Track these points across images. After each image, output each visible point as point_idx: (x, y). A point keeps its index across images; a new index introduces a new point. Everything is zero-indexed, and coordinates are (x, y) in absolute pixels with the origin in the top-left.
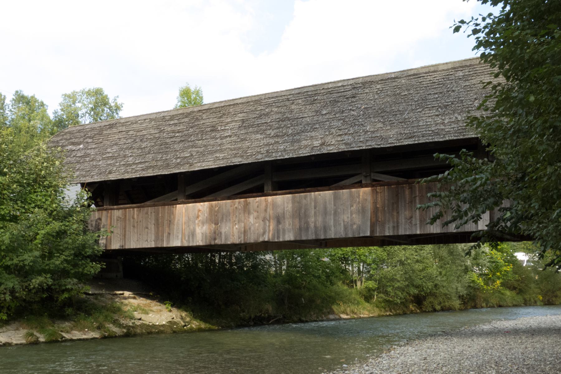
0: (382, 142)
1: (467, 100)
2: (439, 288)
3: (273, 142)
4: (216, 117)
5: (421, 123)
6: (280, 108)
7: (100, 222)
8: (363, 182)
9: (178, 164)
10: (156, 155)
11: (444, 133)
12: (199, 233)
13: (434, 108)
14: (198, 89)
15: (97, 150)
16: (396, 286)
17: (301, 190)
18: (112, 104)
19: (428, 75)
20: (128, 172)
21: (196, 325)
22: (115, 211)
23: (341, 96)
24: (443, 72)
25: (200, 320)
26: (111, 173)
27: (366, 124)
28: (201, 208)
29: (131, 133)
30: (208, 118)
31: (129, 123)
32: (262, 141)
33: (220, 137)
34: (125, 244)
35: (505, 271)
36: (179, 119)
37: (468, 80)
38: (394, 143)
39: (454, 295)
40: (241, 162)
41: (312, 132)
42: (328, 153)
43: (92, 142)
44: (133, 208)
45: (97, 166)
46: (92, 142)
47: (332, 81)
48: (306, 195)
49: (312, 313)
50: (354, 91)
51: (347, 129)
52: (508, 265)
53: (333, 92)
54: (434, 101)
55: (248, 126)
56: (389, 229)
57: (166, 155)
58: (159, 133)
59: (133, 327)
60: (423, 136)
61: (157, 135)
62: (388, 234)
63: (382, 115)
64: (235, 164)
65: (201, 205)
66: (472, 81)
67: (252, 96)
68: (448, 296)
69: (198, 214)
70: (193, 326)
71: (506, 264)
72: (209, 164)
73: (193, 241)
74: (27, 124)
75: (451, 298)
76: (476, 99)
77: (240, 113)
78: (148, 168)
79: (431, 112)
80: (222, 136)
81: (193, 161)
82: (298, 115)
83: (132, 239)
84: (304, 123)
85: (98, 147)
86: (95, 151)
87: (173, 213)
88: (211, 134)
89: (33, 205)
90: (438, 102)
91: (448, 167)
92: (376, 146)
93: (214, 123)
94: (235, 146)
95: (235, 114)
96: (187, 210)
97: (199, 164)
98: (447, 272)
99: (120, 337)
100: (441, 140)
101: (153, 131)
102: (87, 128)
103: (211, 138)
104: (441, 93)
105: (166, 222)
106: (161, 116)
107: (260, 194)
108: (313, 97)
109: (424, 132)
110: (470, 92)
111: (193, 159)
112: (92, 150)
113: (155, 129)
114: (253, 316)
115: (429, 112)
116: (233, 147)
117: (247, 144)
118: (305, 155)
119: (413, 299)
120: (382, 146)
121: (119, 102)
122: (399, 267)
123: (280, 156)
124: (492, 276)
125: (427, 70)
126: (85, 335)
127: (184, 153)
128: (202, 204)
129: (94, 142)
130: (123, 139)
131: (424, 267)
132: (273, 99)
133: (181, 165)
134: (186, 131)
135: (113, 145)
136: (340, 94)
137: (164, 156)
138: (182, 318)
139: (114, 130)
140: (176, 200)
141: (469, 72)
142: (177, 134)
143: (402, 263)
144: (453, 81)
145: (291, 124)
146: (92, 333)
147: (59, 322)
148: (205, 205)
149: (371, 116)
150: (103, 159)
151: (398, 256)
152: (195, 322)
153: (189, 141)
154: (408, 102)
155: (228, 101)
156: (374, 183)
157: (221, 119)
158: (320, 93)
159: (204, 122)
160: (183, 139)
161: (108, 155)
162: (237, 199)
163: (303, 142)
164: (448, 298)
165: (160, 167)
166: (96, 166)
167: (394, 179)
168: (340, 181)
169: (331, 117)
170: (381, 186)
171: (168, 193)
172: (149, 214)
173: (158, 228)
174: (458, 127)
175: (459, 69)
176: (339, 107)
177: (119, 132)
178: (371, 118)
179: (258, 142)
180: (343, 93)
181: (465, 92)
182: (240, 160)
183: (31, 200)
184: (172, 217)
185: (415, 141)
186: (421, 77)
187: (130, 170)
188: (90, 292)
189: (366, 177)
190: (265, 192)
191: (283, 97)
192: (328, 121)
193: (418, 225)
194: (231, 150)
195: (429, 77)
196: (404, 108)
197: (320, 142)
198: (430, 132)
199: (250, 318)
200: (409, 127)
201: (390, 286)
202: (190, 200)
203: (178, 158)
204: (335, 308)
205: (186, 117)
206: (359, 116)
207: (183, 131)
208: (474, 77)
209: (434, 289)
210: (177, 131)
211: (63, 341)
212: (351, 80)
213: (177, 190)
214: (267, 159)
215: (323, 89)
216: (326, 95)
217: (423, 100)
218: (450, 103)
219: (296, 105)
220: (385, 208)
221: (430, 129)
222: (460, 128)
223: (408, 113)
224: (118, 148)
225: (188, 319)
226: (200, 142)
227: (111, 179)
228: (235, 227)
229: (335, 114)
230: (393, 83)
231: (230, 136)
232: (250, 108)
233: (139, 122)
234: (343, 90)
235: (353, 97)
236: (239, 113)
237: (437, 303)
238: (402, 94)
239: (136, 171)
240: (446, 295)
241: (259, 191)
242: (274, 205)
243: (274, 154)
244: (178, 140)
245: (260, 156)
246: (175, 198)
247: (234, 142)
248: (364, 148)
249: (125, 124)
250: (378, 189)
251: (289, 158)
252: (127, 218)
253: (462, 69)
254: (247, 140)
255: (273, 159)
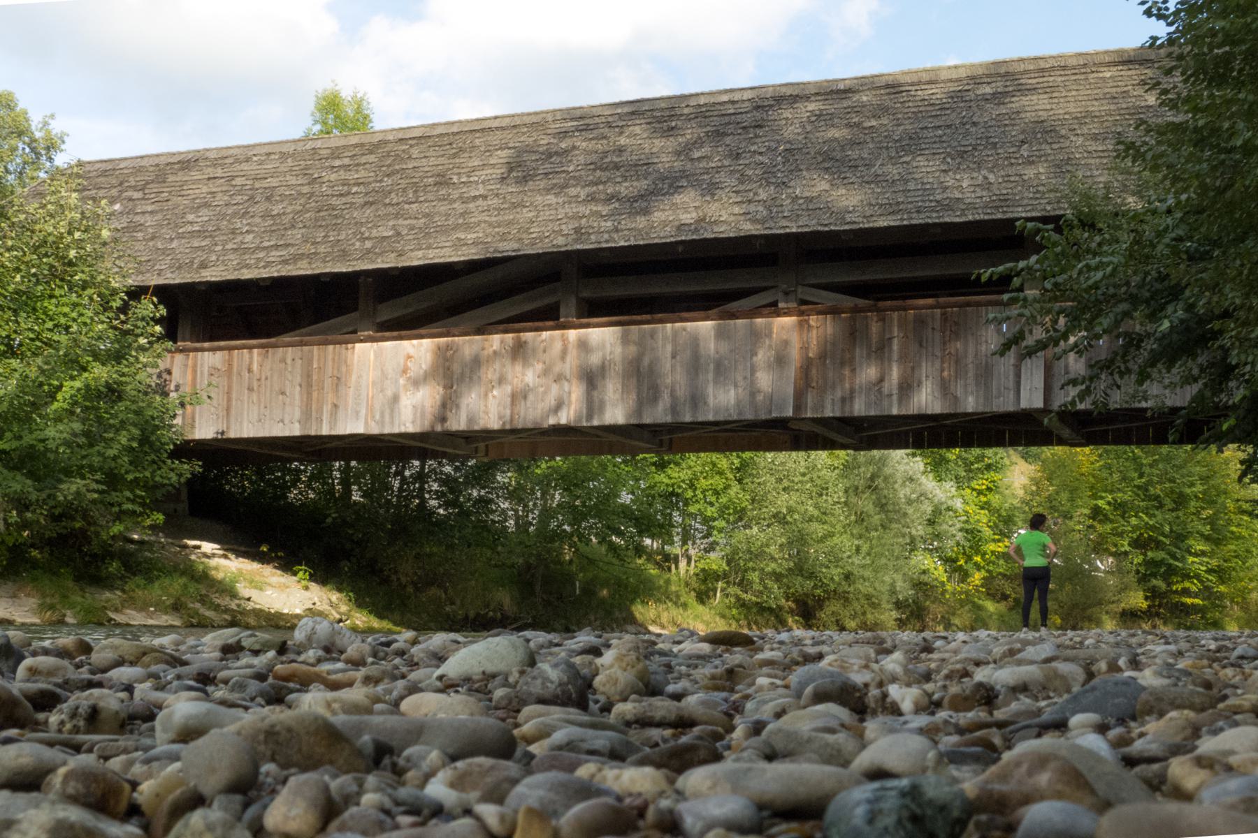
0: (832, 221)
1: (1004, 143)
2: (854, 583)
3: (588, 212)
4: (443, 156)
5: (911, 186)
6: (593, 142)
7: (168, 377)
8: (781, 305)
9: (368, 251)
10: (310, 231)
11: (964, 207)
12: (406, 407)
13: (937, 157)
14: (359, 95)
15: (159, 216)
16: (769, 569)
17: (645, 317)
18: (38, 135)
19: (918, 88)
20: (248, 266)
21: (364, 622)
22: (206, 353)
23: (729, 123)
24: (949, 84)
25: (370, 612)
26: (206, 267)
27: (792, 184)
28: (411, 351)
29: (238, 181)
30: (425, 157)
31: (230, 160)
32: (560, 210)
33: (461, 198)
34: (228, 428)
35: (993, 552)
36: (355, 155)
37: (1004, 104)
38: (859, 223)
39: (885, 597)
40: (519, 250)
41: (672, 194)
42: (716, 239)
43: (143, 199)
44: (250, 348)
45: (168, 252)
46: (143, 199)
47: (706, 90)
48: (654, 329)
49: (592, 618)
50: (757, 114)
51: (750, 190)
52: (999, 541)
53: (711, 114)
54: (935, 142)
55: (524, 177)
56: (833, 404)
57: (336, 233)
58: (309, 184)
59: (241, 613)
60: (918, 212)
61: (305, 189)
62: (831, 415)
63: (826, 165)
64: (505, 254)
65: (414, 346)
66: (1013, 105)
67: (522, 115)
68: (874, 600)
69: (405, 365)
70: (357, 622)
71: (997, 537)
72: (443, 252)
73: (392, 423)
75: (879, 605)
76: (1023, 142)
77: (500, 149)
78: (296, 258)
79: (931, 164)
80: (465, 195)
81: (404, 246)
82: (637, 158)
83: (245, 416)
84: (654, 176)
85: (162, 210)
86: (156, 218)
87: (346, 362)
88: (438, 191)
89: (50, 325)
90: (945, 145)
91: (1038, 248)
92: (820, 228)
93: (440, 167)
94: (500, 218)
95: (488, 151)
96: (378, 355)
97: (420, 254)
98: (871, 548)
100: (958, 220)
101: (293, 181)
102: (121, 166)
103: (440, 200)
104: (949, 127)
105: (328, 382)
106: (308, 147)
107: (550, 323)
108: (665, 121)
109: (920, 204)
110: (1011, 128)
111: (402, 242)
112: (148, 217)
113: (297, 176)
114: (472, 614)
115: (926, 164)
116: (494, 219)
117: (527, 214)
118: (664, 241)
119: (793, 606)
120: (833, 228)
121: (56, 127)
122: (777, 528)
123: (607, 241)
124: (966, 563)
125: (915, 79)
126: (152, 618)
127: (380, 229)
128: (415, 342)
129: (148, 199)
130: (220, 194)
131: (826, 532)
132: (575, 123)
133: (376, 253)
134: (377, 182)
135: (199, 207)
136: (727, 119)
137: (331, 233)
138: (331, 604)
139: (195, 175)
140: (355, 332)
141: (1006, 86)
142: (354, 189)
143: (779, 518)
144: (972, 103)
145: (622, 176)
146: (165, 617)
147: (93, 589)
148: (421, 345)
149: (802, 167)
150: (180, 236)
151: (773, 503)
152: (358, 615)
153: (386, 205)
154: (880, 142)
155: (467, 121)
156: (804, 307)
157: (457, 160)
158: (681, 115)
159: (416, 164)
160: (371, 199)
161: (190, 228)
162: (496, 333)
163: (656, 214)
164: (874, 603)
165: (326, 257)
166: (164, 251)
167: (848, 301)
168: (734, 300)
169: (713, 165)
170: (819, 313)
171: (304, 327)
172: (289, 361)
173: (309, 394)
174: (990, 197)
175: (983, 80)
176: (728, 145)
177: (209, 179)
178: (801, 170)
179: (553, 212)
180: (733, 117)
181: (999, 126)
182: (516, 246)
183: (45, 313)
184: (344, 369)
185: (902, 219)
186: (902, 92)
187: (252, 262)
188: (136, 537)
189: (786, 293)
190: (562, 320)
191: (597, 120)
192: (707, 173)
193: (895, 398)
194: (490, 224)
195: (919, 93)
196: (873, 153)
197: (694, 215)
198: (933, 204)
199: (467, 617)
200: (887, 192)
201: (754, 570)
202: (387, 334)
203: (367, 238)
204: (638, 610)
205: (371, 153)
206: (775, 166)
207: (370, 183)
208: (1017, 99)
209: (844, 583)
210: (352, 182)
212: (749, 91)
213: (356, 309)
214: (579, 247)
215: (687, 106)
216: (696, 120)
217: (911, 138)
218: (970, 148)
219: (628, 137)
220: (825, 361)
221: (931, 198)
222: (994, 198)
223: (882, 165)
224: (212, 213)
225: (344, 608)
226: (412, 206)
227: (209, 279)
228: (490, 395)
229: (720, 160)
230: (844, 101)
231: (485, 197)
232: (522, 139)
233: (255, 159)
234: (732, 111)
235: (756, 127)
236: (497, 150)
237: (848, 614)
238: (867, 124)
239: (268, 265)
240: (868, 597)
241: (548, 316)
242: (583, 345)
243: (592, 237)
244: (359, 200)
245: (560, 241)
246: (351, 329)
247: (494, 208)
248: (794, 230)
249: (220, 162)
250: (813, 320)
251: (630, 246)
252: (235, 370)
253: (989, 80)
254: (525, 207)
255: (591, 246)
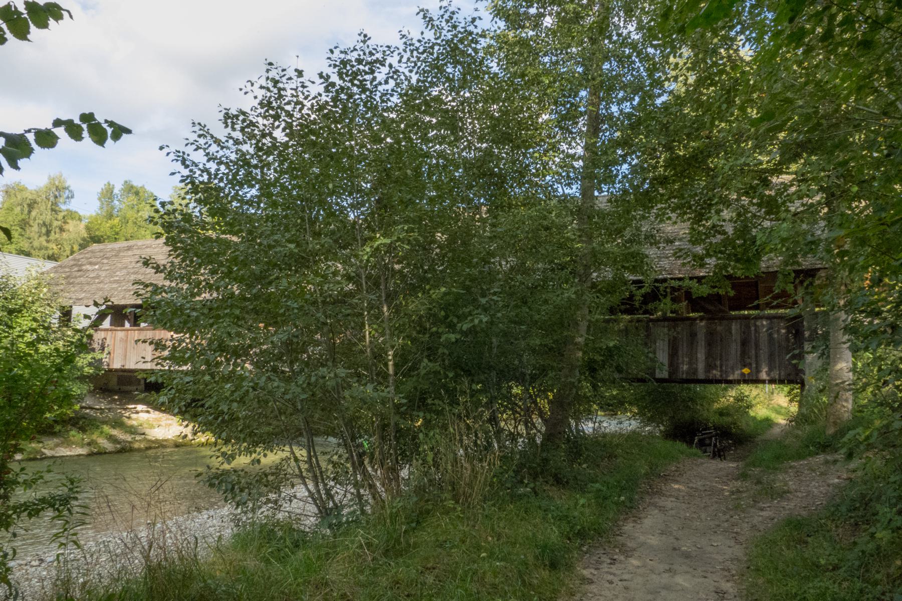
74: (135, 215)
99: (110, 453)
150: (110, 282)
211: (42, 459)
